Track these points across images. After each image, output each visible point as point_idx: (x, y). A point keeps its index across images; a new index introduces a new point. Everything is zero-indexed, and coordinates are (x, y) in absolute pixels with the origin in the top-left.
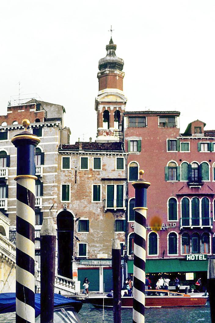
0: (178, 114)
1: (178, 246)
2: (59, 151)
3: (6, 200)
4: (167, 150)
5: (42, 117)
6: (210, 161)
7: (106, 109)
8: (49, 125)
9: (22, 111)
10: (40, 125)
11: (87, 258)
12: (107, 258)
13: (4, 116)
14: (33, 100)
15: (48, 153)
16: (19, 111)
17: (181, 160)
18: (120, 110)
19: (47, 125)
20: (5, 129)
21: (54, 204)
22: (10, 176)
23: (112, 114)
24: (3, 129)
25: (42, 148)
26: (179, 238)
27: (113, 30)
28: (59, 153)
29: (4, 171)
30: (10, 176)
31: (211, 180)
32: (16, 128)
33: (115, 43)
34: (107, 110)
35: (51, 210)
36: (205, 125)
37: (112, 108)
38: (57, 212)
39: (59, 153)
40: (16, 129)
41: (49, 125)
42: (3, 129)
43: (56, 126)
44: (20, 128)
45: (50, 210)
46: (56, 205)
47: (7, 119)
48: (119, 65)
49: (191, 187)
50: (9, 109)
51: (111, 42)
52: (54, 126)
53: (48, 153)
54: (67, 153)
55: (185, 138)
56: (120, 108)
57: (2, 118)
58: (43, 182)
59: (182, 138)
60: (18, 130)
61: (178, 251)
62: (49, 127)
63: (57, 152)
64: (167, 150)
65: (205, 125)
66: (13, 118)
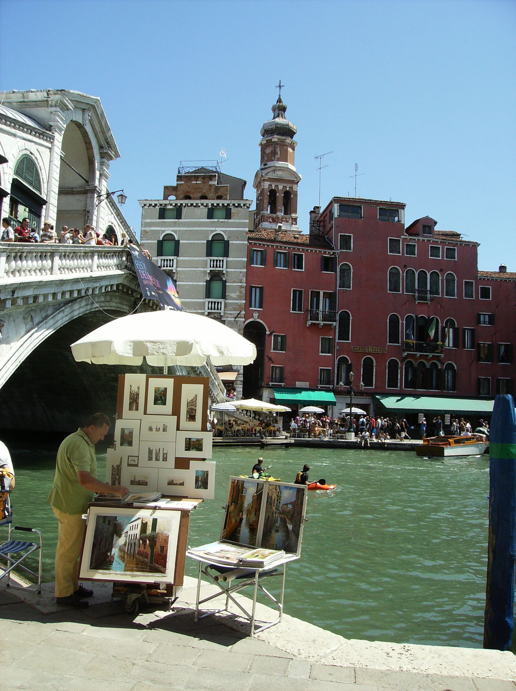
0: (402, 206)
1: (399, 378)
2: (250, 241)
3: (222, 301)
4: (389, 252)
5: (226, 193)
6: (441, 271)
7: (273, 188)
8: (236, 205)
9: (198, 182)
10: (212, 205)
11: (283, 386)
12: (308, 387)
13: (171, 187)
14: (202, 170)
15: (234, 242)
16: (193, 182)
17: (405, 266)
18: (291, 191)
19: (233, 204)
20: (174, 205)
21: (241, 311)
22: (228, 270)
23: (280, 196)
24: (171, 205)
25: (226, 235)
26: (402, 368)
27: (282, 86)
28: (250, 243)
29: (172, 261)
30: (228, 270)
31: (443, 295)
32: (189, 205)
33: (284, 103)
34: (274, 189)
35: (237, 319)
36: (436, 223)
37: (281, 187)
38: (244, 322)
39: (250, 243)
40: (189, 206)
41: (236, 205)
42: (171, 205)
43: (246, 207)
44: (194, 205)
45: (235, 318)
46: (244, 313)
47: (177, 192)
48: (289, 132)
49: (418, 302)
50: (179, 178)
51: (279, 101)
52: (243, 207)
53: (234, 242)
54: (260, 244)
55: (411, 239)
56: (291, 188)
57: (169, 189)
58: (226, 281)
59: (407, 239)
60: (192, 207)
61: (399, 384)
62: (237, 207)
63: (247, 242)
64: (389, 252)
65: (436, 223)
66: (185, 191)
